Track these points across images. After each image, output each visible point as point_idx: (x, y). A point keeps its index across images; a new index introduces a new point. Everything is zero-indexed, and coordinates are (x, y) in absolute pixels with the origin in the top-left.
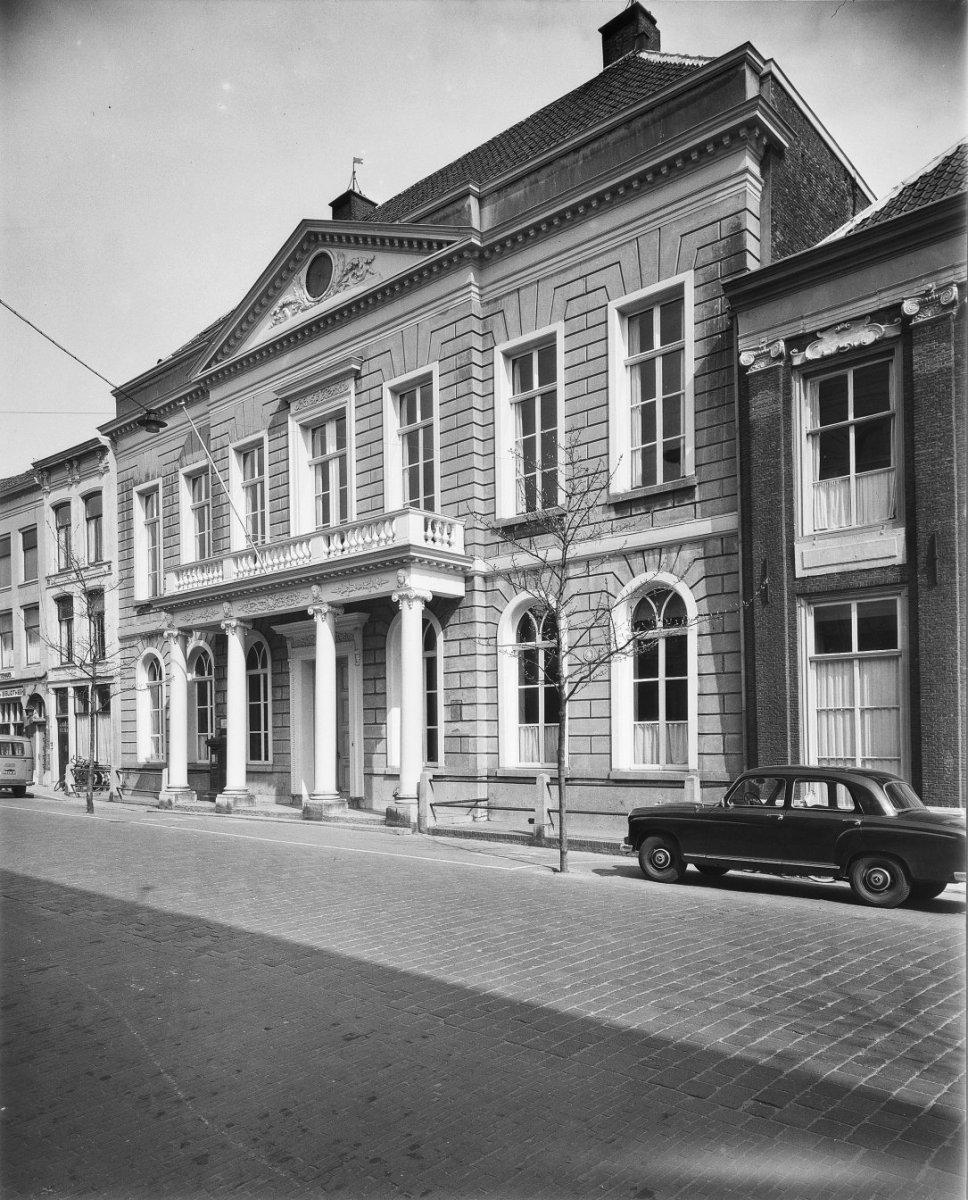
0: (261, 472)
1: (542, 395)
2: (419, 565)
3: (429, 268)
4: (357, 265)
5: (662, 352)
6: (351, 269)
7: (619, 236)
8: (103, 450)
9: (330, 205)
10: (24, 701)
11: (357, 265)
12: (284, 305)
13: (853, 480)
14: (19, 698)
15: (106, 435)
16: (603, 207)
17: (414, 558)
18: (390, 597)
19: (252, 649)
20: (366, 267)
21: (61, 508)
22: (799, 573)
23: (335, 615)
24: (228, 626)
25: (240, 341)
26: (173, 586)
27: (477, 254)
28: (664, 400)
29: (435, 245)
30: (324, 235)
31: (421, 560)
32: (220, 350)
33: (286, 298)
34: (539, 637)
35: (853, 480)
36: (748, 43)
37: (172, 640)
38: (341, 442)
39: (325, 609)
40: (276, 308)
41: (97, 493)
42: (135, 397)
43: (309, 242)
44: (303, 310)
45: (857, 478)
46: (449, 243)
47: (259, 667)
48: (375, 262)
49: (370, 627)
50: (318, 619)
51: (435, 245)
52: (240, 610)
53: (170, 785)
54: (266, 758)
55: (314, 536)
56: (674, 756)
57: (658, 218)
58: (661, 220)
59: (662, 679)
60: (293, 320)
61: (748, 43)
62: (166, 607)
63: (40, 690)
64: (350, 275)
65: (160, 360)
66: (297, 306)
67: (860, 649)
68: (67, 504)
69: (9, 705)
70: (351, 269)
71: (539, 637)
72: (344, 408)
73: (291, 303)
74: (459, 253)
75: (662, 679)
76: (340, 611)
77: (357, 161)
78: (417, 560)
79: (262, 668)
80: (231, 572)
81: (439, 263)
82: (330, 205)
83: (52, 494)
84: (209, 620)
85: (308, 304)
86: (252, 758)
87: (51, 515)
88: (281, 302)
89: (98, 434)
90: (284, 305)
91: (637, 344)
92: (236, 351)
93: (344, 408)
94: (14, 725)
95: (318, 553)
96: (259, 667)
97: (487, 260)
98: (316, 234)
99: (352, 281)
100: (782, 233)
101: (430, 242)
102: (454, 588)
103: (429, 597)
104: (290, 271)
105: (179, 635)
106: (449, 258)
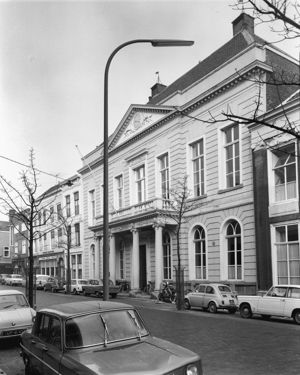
0: (167, 165)
1: (235, 144)
2: (160, 216)
3: (169, 117)
4: (147, 118)
5: (201, 157)
6: (146, 119)
7: (221, 105)
8: (79, 178)
9: (232, 23)
10: (58, 260)
11: (147, 118)
12: (128, 131)
13: (286, 185)
14: (56, 259)
15: (80, 173)
17: (158, 214)
18: (130, 231)
19: (164, 235)
20: (150, 118)
21: (68, 197)
22: (270, 216)
23: (139, 232)
24: (133, 231)
28: (235, 158)
33: (128, 129)
34: (234, 233)
35: (286, 185)
37: (111, 237)
39: (135, 230)
40: (125, 132)
41: (69, 196)
44: (133, 132)
45: (287, 184)
46: (171, 111)
47: (201, 237)
48: (152, 116)
49: (147, 234)
50: (134, 233)
52: (137, 225)
54: (170, 278)
55: (154, 200)
56: (239, 278)
57: (231, 99)
58: (232, 100)
59: (236, 251)
60: (130, 136)
62: (93, 230)
63: (62, 256)
64: (145, 121)
65: (97, 146)
67: (288, 241)
68: (69, 196)
69: (54, 261)
70: (146, 119)
71: (234, 233)
73: (129, 130)
75: (236, 251)
77: (157, 73)
78: (159, 215)
79: (202, 238)
82: (232, 23)
83: (73, 189)
84: (148, 225)
85: (134, 130)
86: (165, 278)
87: (65, 199)
89: (77, 173)
90: (128, 131)
91: (138, 179)
92: (115, 145)
94: (46, 268)
96: (201, 237)
99: (146, 123)
100: (272, 100)
101: (166, 110)
102: (172, 222)
105: (136, 231)
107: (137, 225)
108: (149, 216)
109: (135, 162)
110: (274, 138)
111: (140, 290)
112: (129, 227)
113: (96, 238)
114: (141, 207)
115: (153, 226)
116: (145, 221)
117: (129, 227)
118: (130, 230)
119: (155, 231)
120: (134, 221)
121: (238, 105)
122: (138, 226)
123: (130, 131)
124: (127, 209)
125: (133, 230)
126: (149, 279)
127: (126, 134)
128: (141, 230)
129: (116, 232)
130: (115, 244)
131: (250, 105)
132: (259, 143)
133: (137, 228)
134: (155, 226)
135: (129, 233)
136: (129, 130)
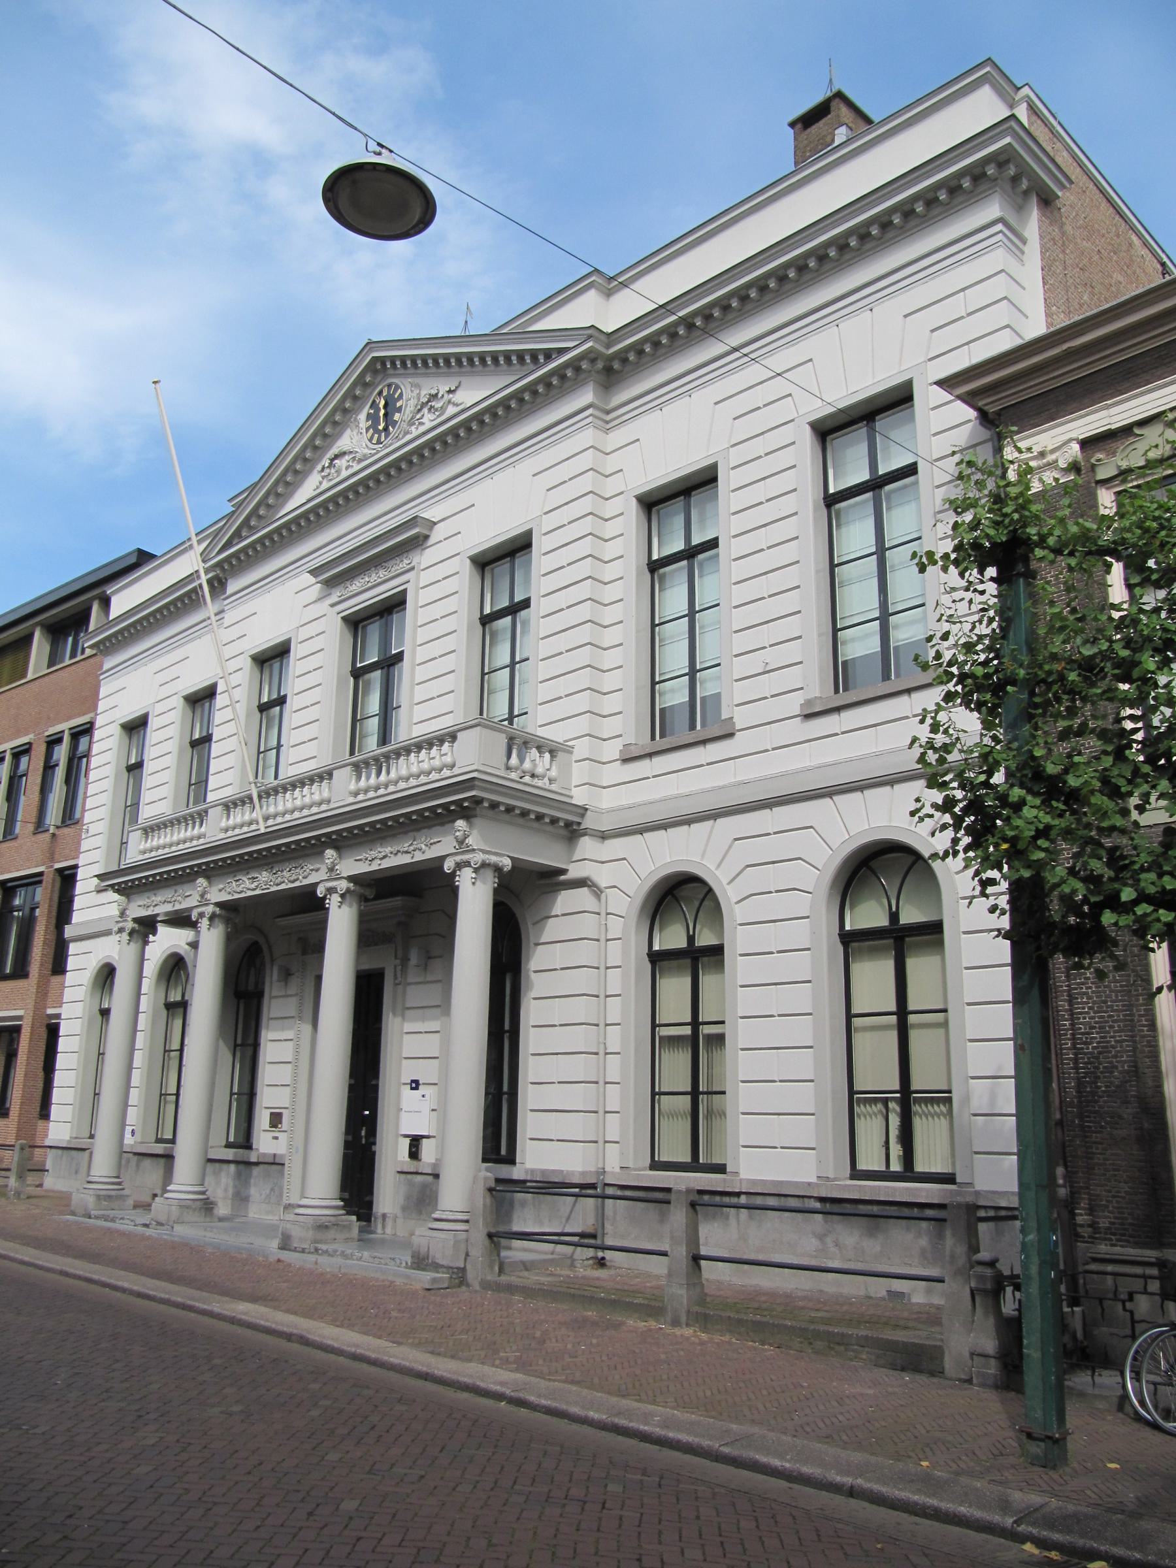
2: (490, 813)
3: (531, 388)
12: (336, 457)
16: (767, 298)
18: (442, 867)
23: (363, 899)
24: (331, 891)
25: (282, 498)
26: (138, 850)
27: (600, 365)
29: (541, 359)
30: (393, 359)
31: (494, 806)
32: (246, 522)
36: (989, 59)
38: (559, 1381)
40: (326, 462)
42: (638, 286)
43: (375, 372)
49: (408, 912)
51: (541, 359)
52: (355, 864)
53: (90, 1179)
60: (346, 470)
61: (989, 59)
64: (425, 410)
66: (357, 445)
72: (405, 590)
73: (344, 454)
74: (575, 364)
76: (370, 893)
80: (215, 829)
81: (545, 380)
88: (330, 454)
90: (336, 457)
93: (405, 590)
95: (345, 792)
97: (617, 372)
98: (383, 360)
103: (507, 863)
104: (346, 411)
105: (348, 891)
106: (559, 372)
107: (355, 864)
108: (432, 809)
109: (356, 585)
110: (1137, 431)
111: (343, 1208)
112: (312, 874)
113: (130, 925)
114: (374, 772)
115: (448, 866)
116: (167, 894)
117: (312, 874)
118: (442, 859)
119: (455, 891)
120: (343, 842)
121: (905, 316)
122: (225, 897)
123: (347, 457)
124: (312, 780)
125: (200, 910)
126: (1153, 1260)
127: (327, 471)
128: (374, 890)
129: (237, 896)
130: (523, 936)
131: (970, 310)
132: (1050, 458)
133: (351, 879)
134: (201, 915)
135: (309, 904)
136: (344, 454)
